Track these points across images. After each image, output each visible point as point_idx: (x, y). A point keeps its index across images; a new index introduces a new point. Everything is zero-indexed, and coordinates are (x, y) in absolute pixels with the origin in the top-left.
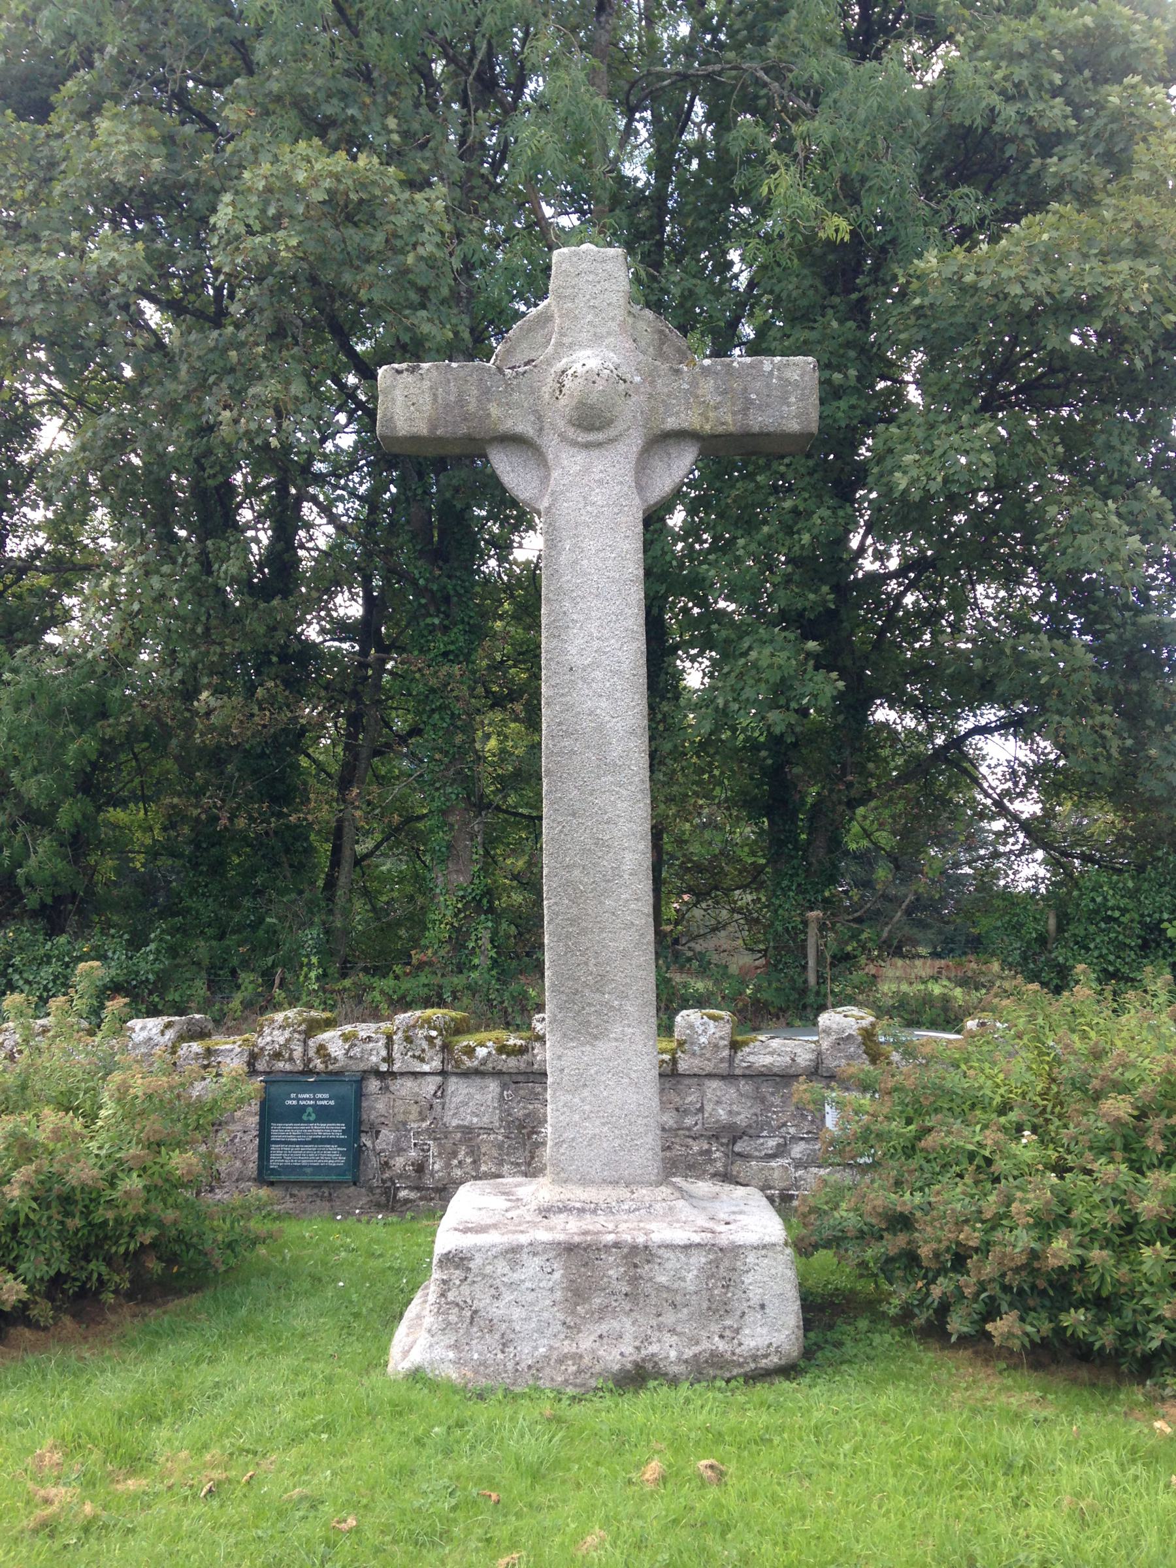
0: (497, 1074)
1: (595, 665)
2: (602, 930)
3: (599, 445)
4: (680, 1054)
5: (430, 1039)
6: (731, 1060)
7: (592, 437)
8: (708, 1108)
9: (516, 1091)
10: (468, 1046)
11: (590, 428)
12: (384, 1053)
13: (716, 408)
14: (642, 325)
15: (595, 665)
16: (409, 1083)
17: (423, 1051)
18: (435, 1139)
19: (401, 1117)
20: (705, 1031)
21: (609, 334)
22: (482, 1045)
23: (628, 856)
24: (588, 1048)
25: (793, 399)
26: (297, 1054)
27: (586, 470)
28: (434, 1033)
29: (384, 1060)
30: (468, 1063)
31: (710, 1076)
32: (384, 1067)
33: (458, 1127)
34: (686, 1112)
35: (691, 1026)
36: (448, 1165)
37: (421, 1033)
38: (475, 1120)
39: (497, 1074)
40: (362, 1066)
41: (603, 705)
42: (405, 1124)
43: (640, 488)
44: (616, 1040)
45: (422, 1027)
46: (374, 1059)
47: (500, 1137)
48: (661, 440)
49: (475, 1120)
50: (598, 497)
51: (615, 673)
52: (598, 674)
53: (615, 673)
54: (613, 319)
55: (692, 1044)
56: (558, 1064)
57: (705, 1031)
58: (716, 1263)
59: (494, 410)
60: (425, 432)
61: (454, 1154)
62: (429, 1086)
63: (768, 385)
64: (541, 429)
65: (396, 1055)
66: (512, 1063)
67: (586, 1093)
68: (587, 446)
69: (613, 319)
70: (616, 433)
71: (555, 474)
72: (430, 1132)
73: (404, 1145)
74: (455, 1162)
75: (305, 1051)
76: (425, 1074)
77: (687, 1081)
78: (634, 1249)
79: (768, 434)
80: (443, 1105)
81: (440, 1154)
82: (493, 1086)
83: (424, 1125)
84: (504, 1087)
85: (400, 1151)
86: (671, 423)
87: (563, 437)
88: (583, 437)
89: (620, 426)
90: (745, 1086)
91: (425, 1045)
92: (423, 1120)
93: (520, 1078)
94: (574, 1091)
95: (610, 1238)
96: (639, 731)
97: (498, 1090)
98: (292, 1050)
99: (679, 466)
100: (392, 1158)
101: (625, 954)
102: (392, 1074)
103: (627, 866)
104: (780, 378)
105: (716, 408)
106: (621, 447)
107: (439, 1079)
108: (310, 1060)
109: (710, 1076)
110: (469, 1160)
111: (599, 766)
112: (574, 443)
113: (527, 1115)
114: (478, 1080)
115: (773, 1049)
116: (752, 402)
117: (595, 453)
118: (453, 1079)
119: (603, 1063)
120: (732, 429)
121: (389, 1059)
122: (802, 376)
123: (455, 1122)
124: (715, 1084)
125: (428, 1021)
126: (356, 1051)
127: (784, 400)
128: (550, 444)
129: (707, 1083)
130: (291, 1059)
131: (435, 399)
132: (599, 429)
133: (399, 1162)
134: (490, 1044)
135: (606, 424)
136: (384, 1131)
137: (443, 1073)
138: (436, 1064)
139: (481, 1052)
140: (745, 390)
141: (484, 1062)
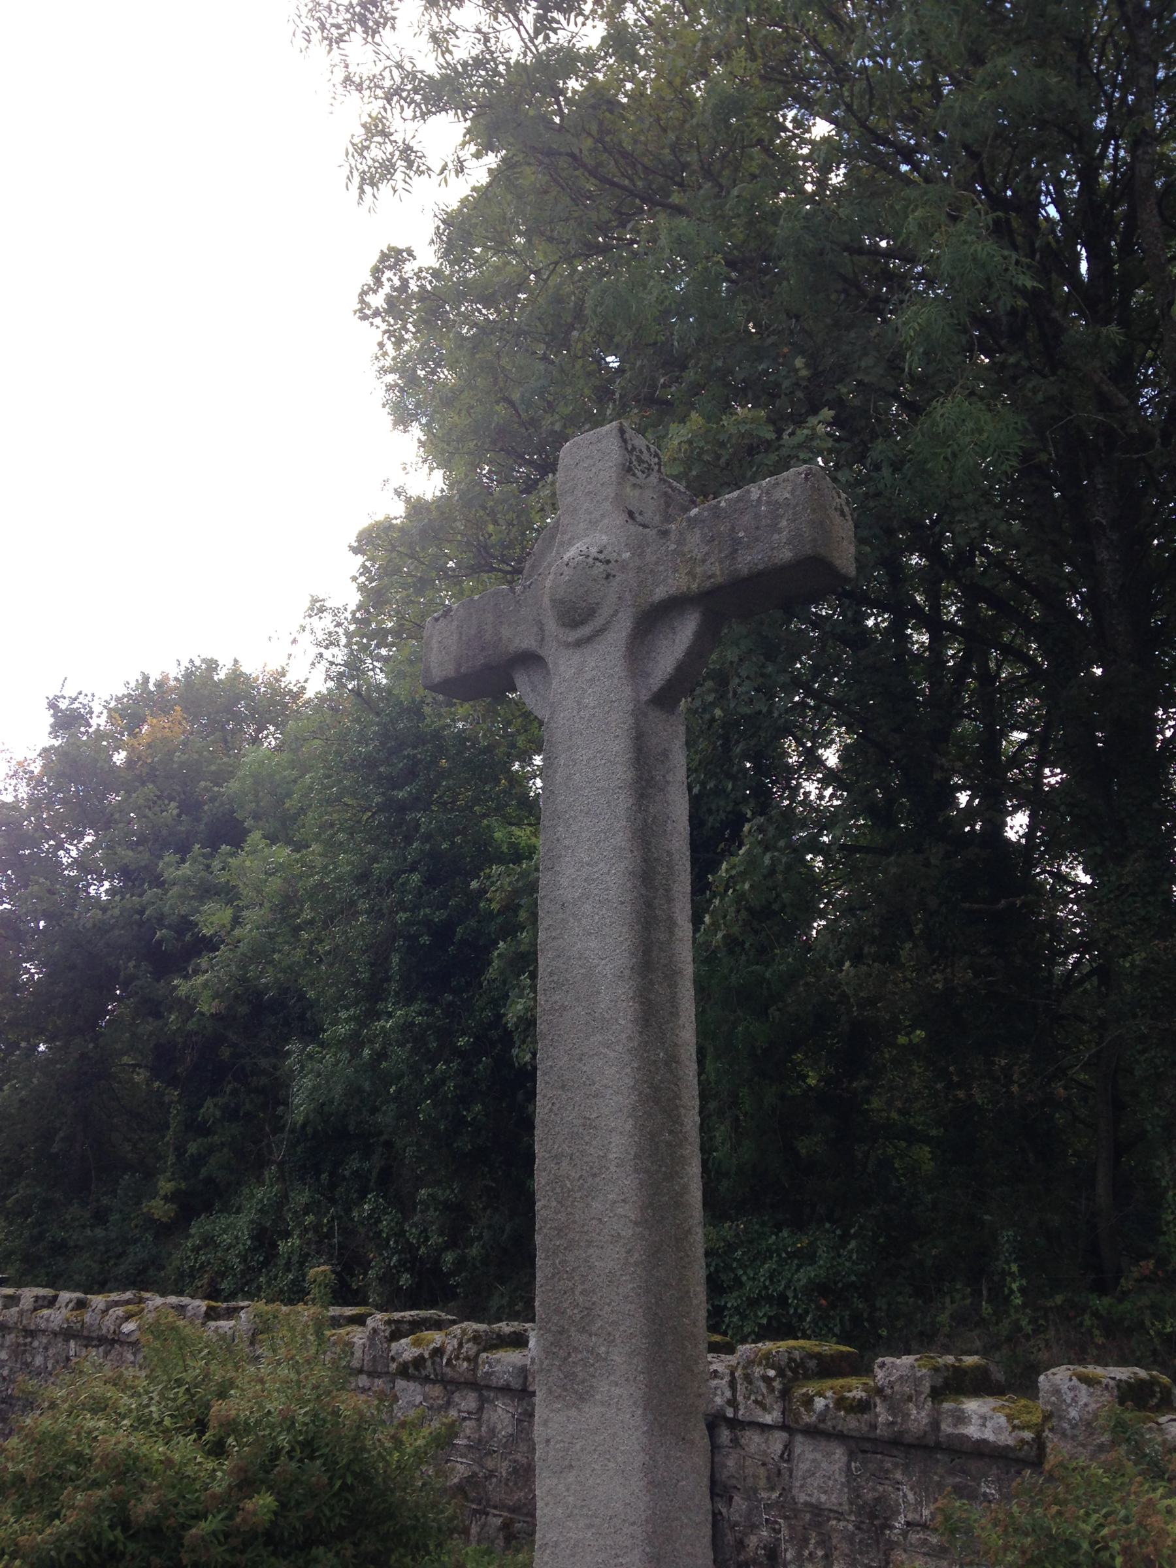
0: (840, 1437)
2: (589, 1244)
3: (589, 639)
4: (1047, 1433)
5: (767, 1380)
7: (585, 631)
10: (806, 1394)
12: (728, 1394)
13: (704, 561)
20: (1074, 1400)
21: (603, 516)
22: (821, 1394)
23: (616, 1139)
24: (573, 1412)
25: (784, 523)
28: (772, 1373)
30: (808, 1419)
33: (806, 1504)
35: (1057, 1392)
37: (758, 1371)
38: (823, 1498)
39: (840, 1437)
41: (592, 944)
42: (755, 1491)
44: (602, 1403)
45: (760, 1364)
47: (850, 1527)
49: (823, 1498)
52: (587, 908)
54: (606, 498)
55: (1061, 1418)
57: (1074, 1400)
59: (506, 632)
60: (452, 674)
63: (757, 516)
64: (543, 639)
66: (852, 1423)
67: (571, 1477)
69: (606, 498)
70: (602, 622)
72: (779, 1505)
74: (806, 1553)
79: (760, 574)
80: (791, 1470)
81: (791, 1538)
83: (775, 1495)
84: (851, 1455)
86: (660, 593)
89: (605, 612)
92: (772, 1489)
93: (868, 1446)
96: (627, 972)
97: (845, 1459)
100: (746, 1535)
104: (768, 503)
105: (704, 561)
110: (820, 1553)
111: (588, 1022)
113: (877, 1500)
116: (738, 541)
120: (720, 580)
122: (793, 492)
125: (768, 1356)
127: (774, 528)
128: (549, 652)
132: (582, 623)
133: (753, 1541)
134: (829, 1394)
135: (591, 613)
139: (820, 1403)
140: (733, 529)
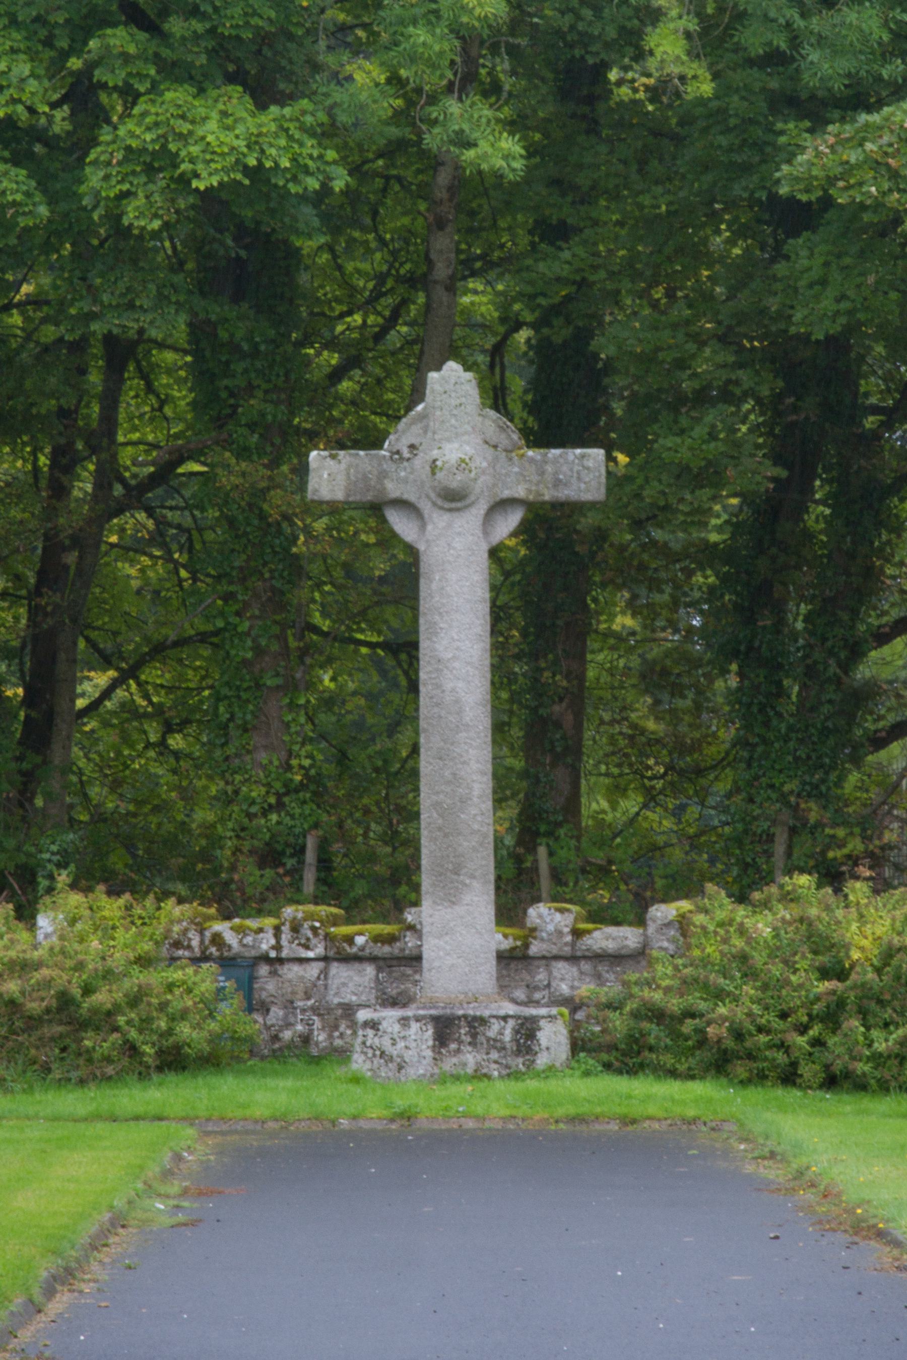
0: (373, 959)
1: (455, 658)
3: (458, 510)
5: (314, 929)
6: (573, 944)
7: (453, 505)
8: (554, 984)
9: (390, 973)
11: (453, 500)
12: (273, 942)
14: (488, 423)
15: (455, 658)
16: (296, 968)
17: (308, 939)
18: (319, 1015)
19: (289, 997)
23: (476, 786)
26: (195, 943)
27: (449, 526)
29: (273, 948)
31: (557, 958)
32: (273, 954)
33: (340, 1004)
34: (537, 988)
36: (330, 1036)
38: (354, 998)
39: (373, 959)
40: (253, 953)
42: (292, 1002)
43: (486, 533)
46: (264, 947)
48: (501, 505)
49: (354, 998)
50: (458, 543)
51: (468, 663)
52: (456, 664)
53: (468, 663)
56: (430, 920)
58: (522, 1025)
61: (336, 1027)
62: (313, 970)
65: (284, 942)
67: (447, 938)
68: (450, 510)
71: (429, 527)
72: (314, 1010)
73: (292, 1020)
75: (202, 942)
76: (308, 960)
77: (536, 963)
78: (475, 1018)
82: (370, 970)
84: (379, 970)
85: (289, 1025)
86: (506, 494)
87: (434, 504)
88: (447, 505)
90: (586, 966)
91: (310, 934)
92: (308, 999)
93: (395, 962)
94: (440, 937)
95: (461, 1012)
98: (190, 940)
99: (512, 520)
100: (281, 1031)
101: (474, 849)
102: (280, 961)
103: (476, 793)
106: (474, 511)
107: (321, 964)
108: (207, 948)
109: (557, 958)
112: (441, 508)
113: (400, 994)
114: (357, 965)
115: (605, 938)
117: (456, 514)
118: (335, 964)
119: (457, 933)
121: (278, 947)
123: (336, 1001)
124: (561, 965)
126: (249, 940)
129: (554, 963)
130: (189, 947)
131: (348, 478)
136: (274, 1009)
137: (325, 959)
138: (320, 950)
139: (360, 940)
141: (362, 949)
